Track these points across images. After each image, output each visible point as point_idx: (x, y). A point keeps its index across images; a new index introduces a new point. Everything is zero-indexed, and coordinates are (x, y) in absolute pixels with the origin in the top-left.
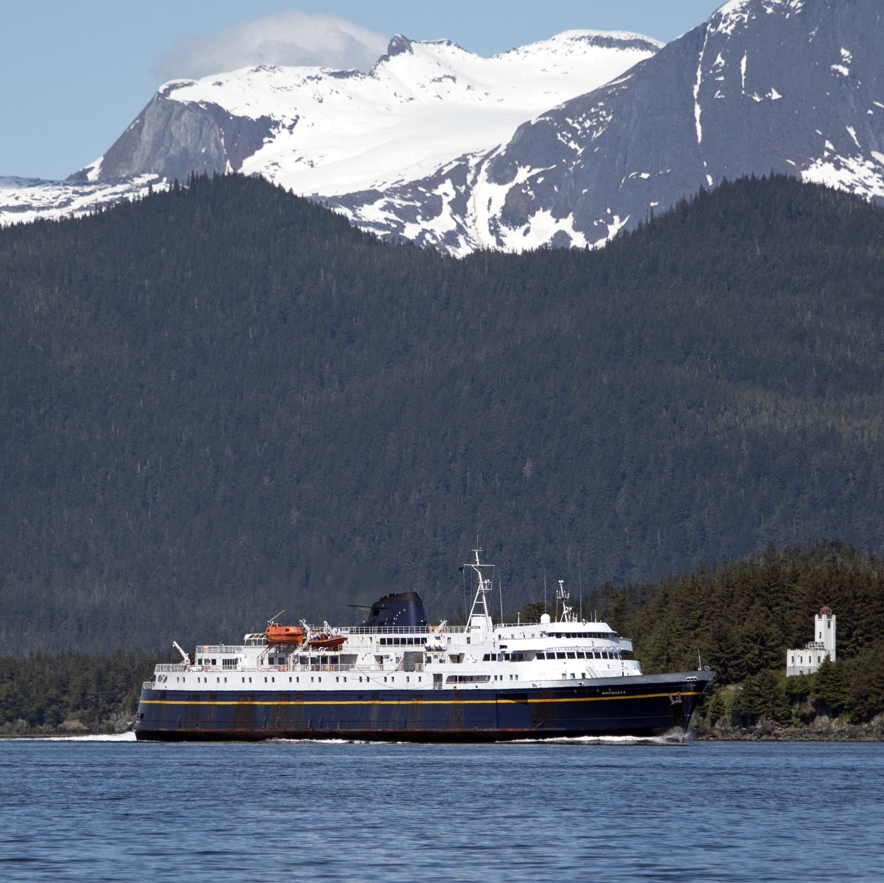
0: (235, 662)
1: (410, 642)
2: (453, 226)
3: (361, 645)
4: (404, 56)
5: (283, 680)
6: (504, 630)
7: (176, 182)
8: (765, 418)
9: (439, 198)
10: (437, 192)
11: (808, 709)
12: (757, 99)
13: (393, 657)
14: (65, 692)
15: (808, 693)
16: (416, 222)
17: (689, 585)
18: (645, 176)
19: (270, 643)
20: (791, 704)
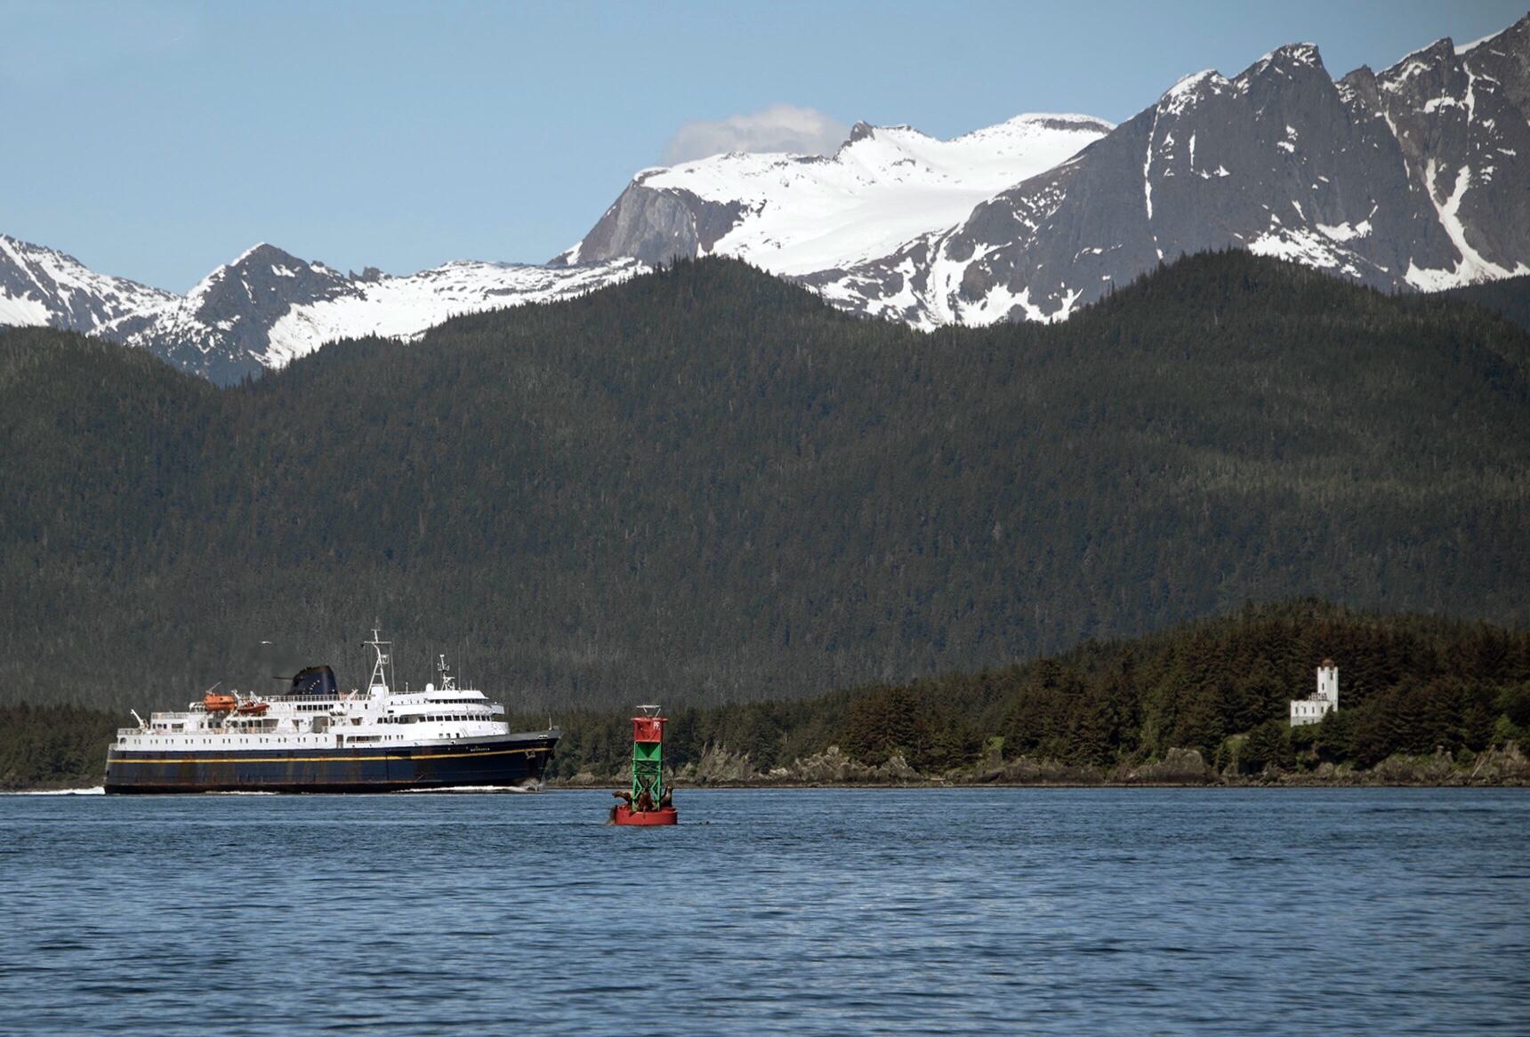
0: (181, 726)
2: (913, 302)
4: (866, 141)
6: (397, 698)
8: (1225, 480)
10: (897, 270)
11: (1313, 756)
12: (1206, 176)
14: (577, 747)
18: (1097, 251)
19: (209, 711)
20: (1296, 752)
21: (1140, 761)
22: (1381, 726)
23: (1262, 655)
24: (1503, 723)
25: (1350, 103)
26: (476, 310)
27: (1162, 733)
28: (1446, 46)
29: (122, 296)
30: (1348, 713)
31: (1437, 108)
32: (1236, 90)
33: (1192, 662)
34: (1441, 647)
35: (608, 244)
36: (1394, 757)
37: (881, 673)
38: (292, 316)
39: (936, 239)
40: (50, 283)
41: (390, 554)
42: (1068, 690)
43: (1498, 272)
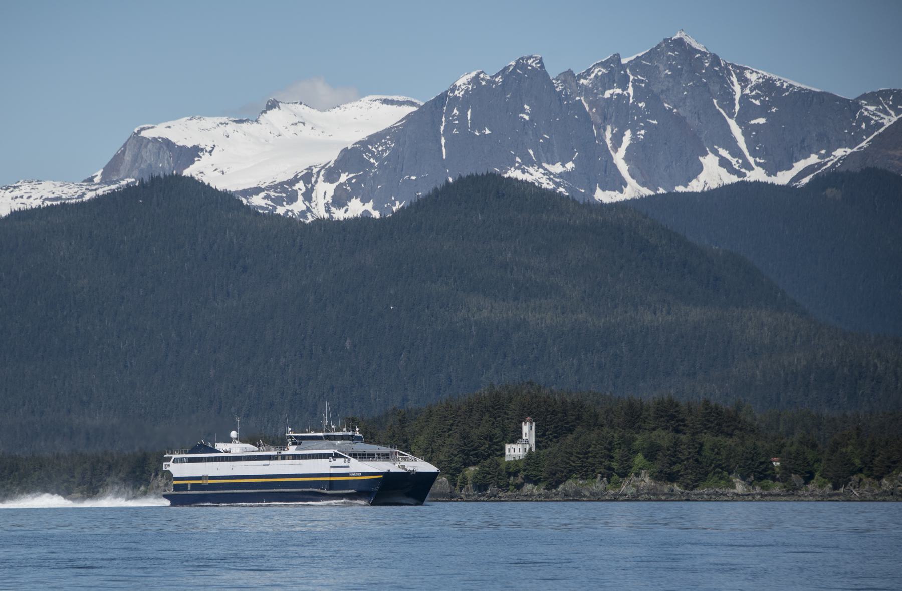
2: (304, 208)
4: (275, 111)
8: (485, 313)
10: (294, 188)
11: (519, 480)
12: (477, 134)
15: (519, 471)
16: (283, 205)
17: (445, 405)
18: (414, 178)
20: (509, 477)
24: (639, 459)
25: (561, 91)
28: (617, 58)
30: (542, 452)
31: (612, 95)
32: (494, 82)
36: (570, 481)
37: (277, 430)
39: (317, 170)
43: (646, 192)
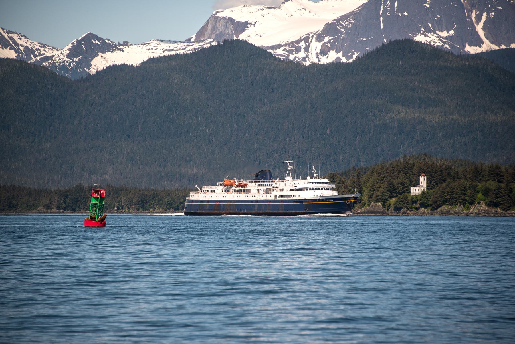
0: (214, 191)
1: (268, 185)
2: (305, 56)
3: (253, 186)
5: (229, 197)
6: (296, 182)
7: (219, 42)
8: (402, 115)
9: (300, 47)
10: (299, 45)
11: (418, 205)
12: (400, 15)
13: (262, 190)
18: (365, 39)
19: (225, 186)
20: (412, 204)
21: (361, 207)
22: (440, 196)
23: (402, 172)
24: (480, 195)
26: (158, 56)
27: (369, 198)
29: (42, 49)
30: (429, 191)
33: (379, 174)
34: (460, 170)
35: (204, 35)
38: (99, 57)
39: (312, 35)
40: (17, 44)
41: (129, 136)
42: (339, 183)
43: (495, 47)
